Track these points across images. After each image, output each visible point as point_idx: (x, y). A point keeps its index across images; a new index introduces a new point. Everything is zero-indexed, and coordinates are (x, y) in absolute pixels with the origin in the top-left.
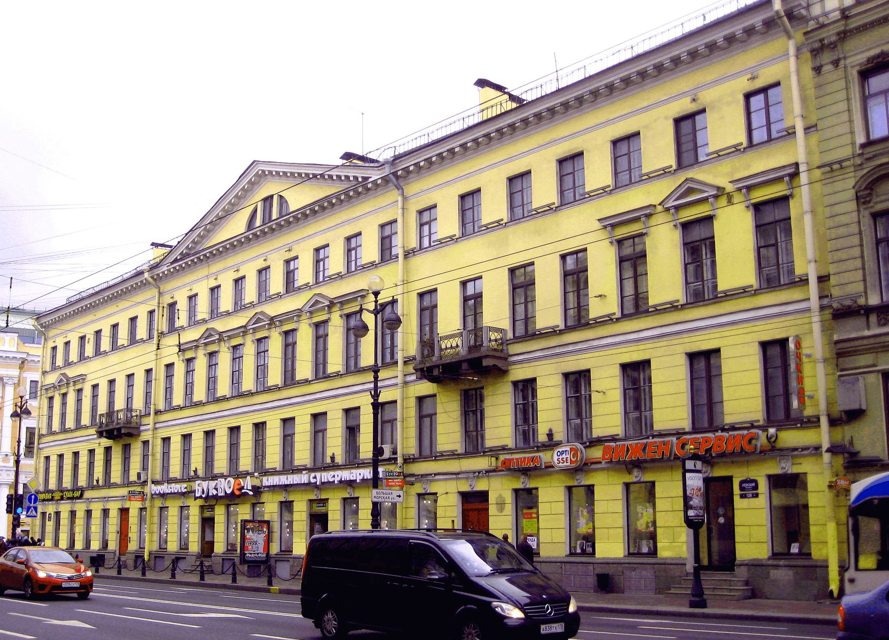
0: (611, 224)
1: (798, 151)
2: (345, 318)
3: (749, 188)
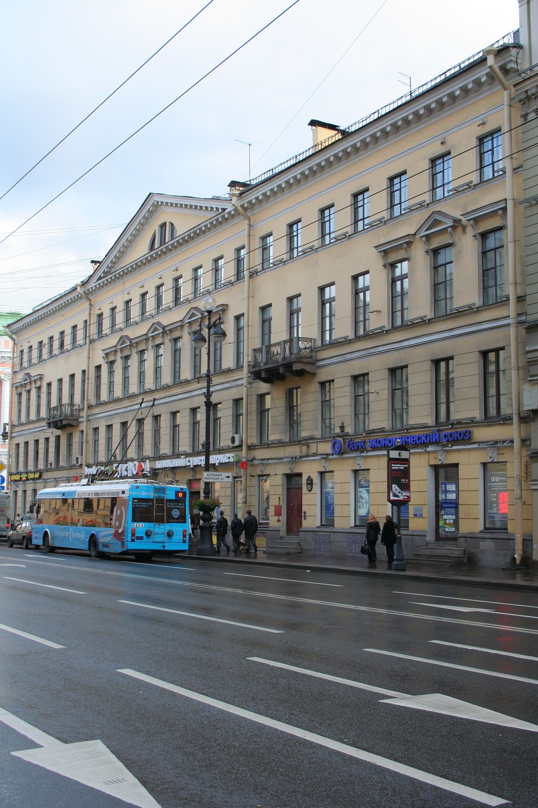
1: (505, 191)
2: (431, 253)
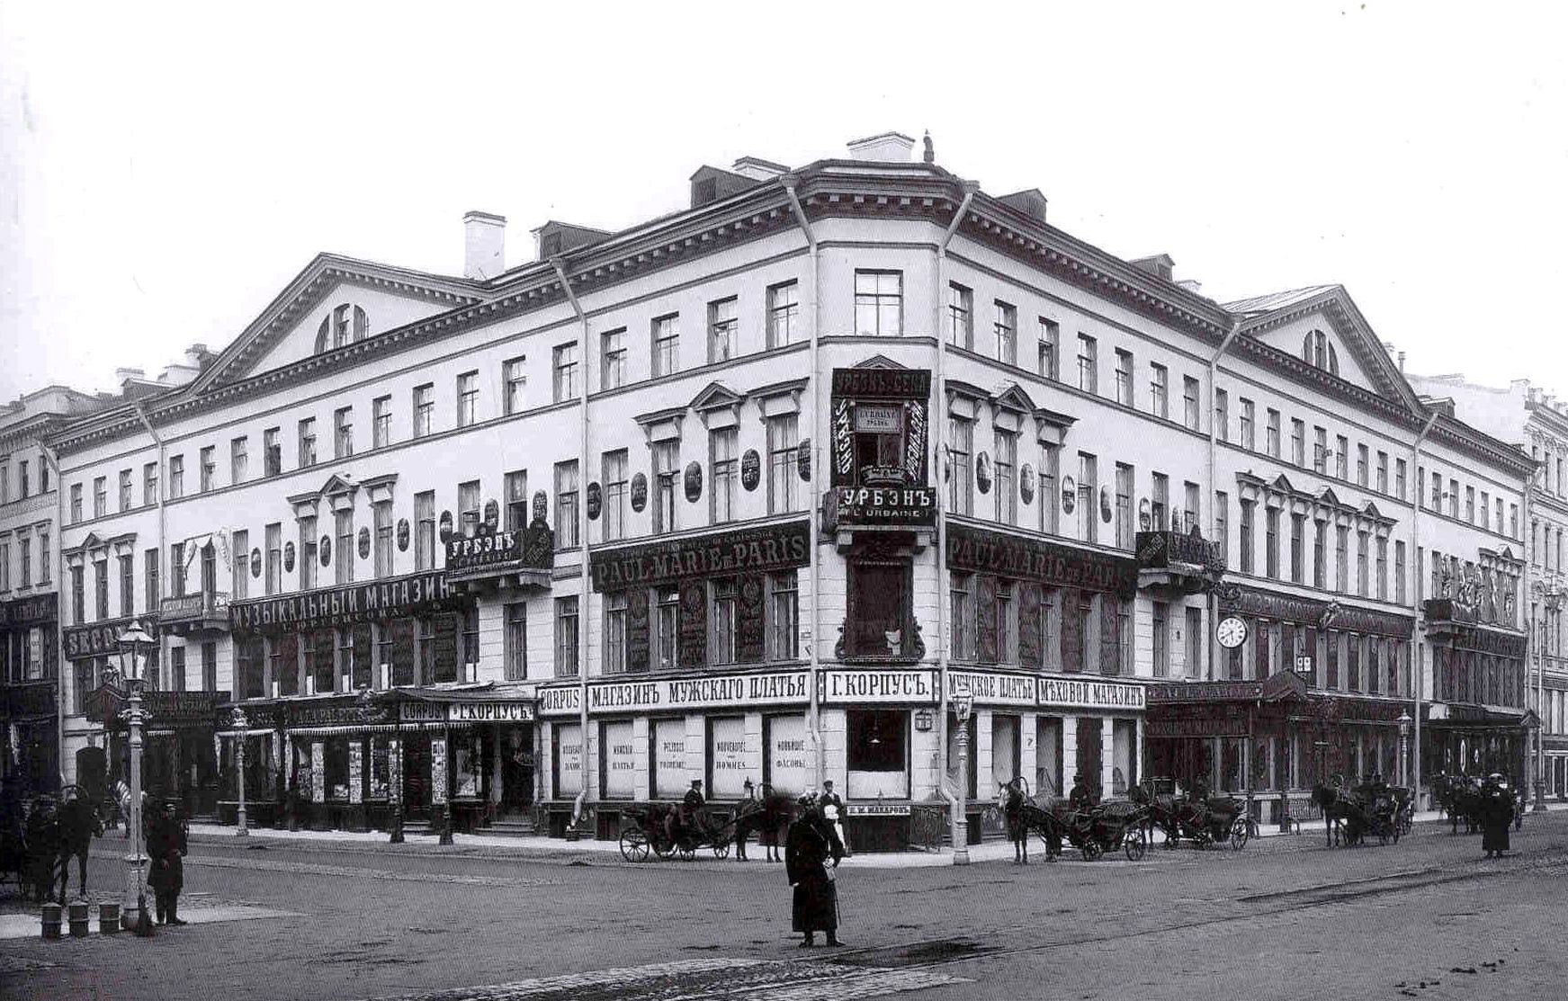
0: (650, 421)
3: (373, 488)
